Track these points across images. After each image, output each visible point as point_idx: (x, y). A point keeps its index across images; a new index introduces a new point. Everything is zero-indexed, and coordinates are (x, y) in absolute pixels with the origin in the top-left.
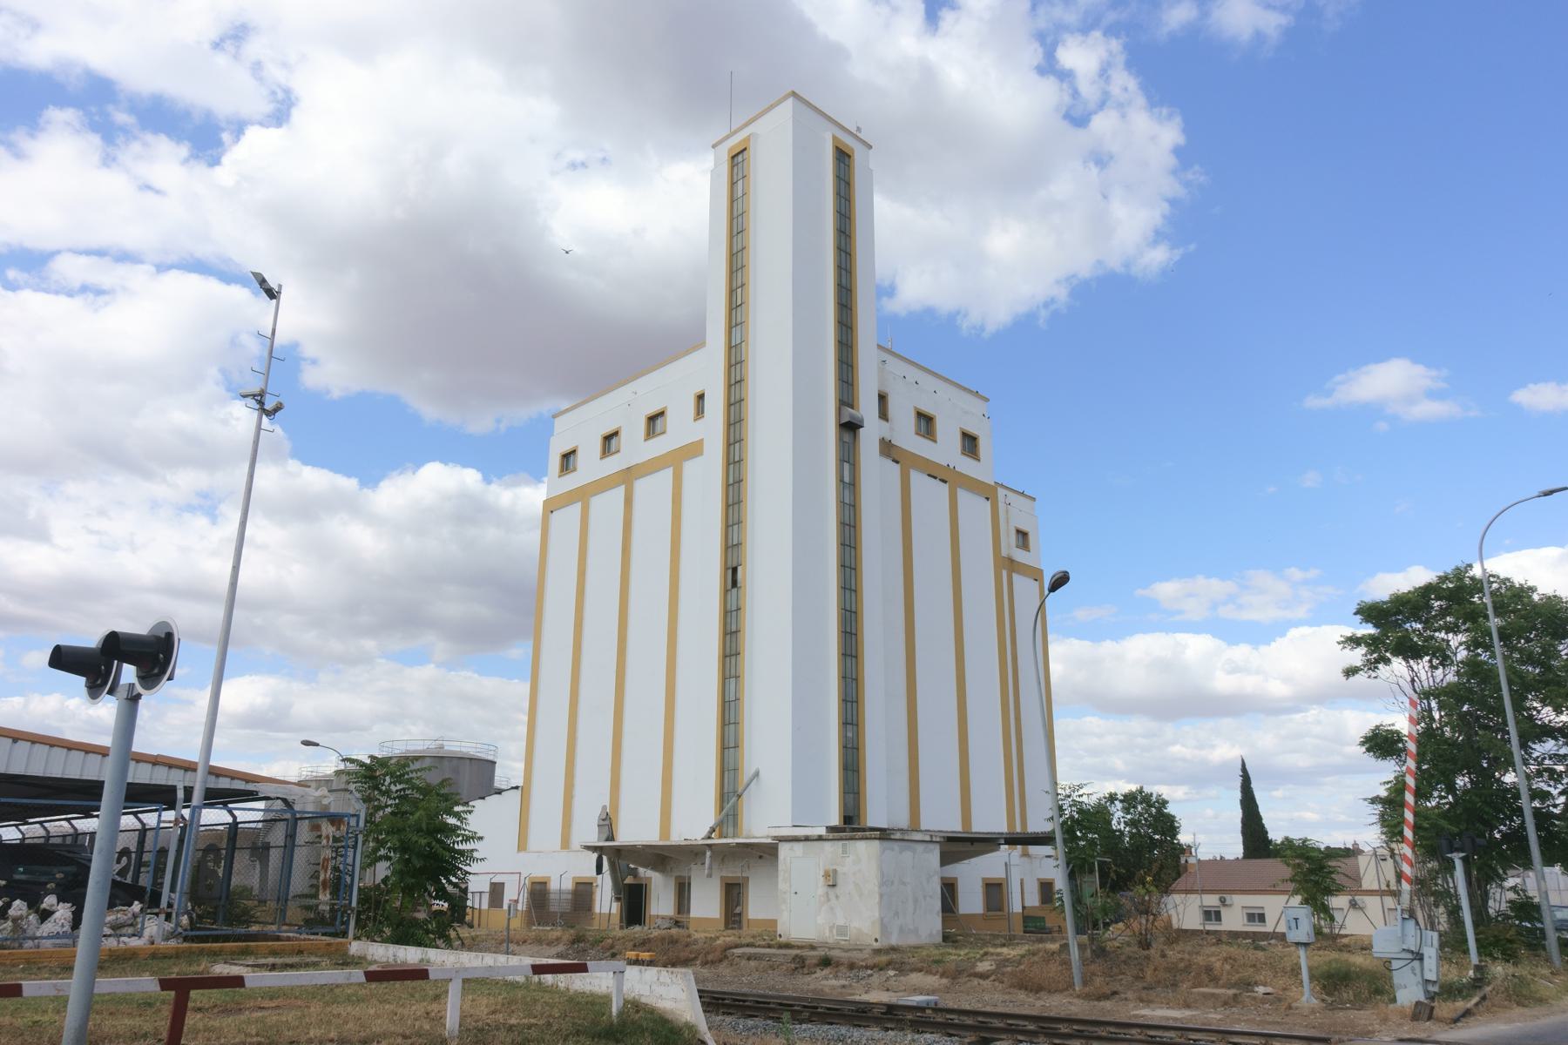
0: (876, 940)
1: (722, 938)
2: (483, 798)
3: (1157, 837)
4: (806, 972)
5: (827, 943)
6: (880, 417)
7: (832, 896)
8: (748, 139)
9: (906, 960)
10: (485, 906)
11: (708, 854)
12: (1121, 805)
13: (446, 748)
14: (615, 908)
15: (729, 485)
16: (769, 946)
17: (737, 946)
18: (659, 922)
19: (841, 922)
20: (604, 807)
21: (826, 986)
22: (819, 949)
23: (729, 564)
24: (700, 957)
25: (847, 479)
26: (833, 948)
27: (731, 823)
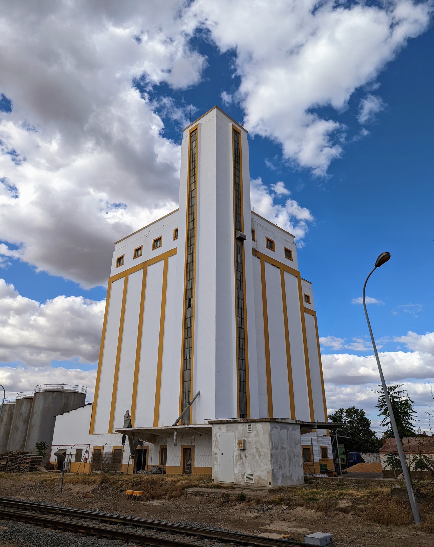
0: (270, 484)
1: (181, 481)
2: (76, 409)
3: (361, 428)
4: (230, 505)
5: (240, 485)
6: (252, 240)
7: (243, 456)
8: (198, 125)
9: (291, 498)
10: (73, 461)
11: (175, 433)
12: (345, 414)
13: (65, 388)
14: (132, 461)
15: (189, 230)
16: (208, 487)
17: (189, 487)
18: (152, 468)
19: (248, 472)
20: (128, 411)
21: (244, 517)
22: (237, 489)
23: (188, 297)
24: (168, 493)
25: (239, 261)
26: (245, 489)
27: (186, 418)
